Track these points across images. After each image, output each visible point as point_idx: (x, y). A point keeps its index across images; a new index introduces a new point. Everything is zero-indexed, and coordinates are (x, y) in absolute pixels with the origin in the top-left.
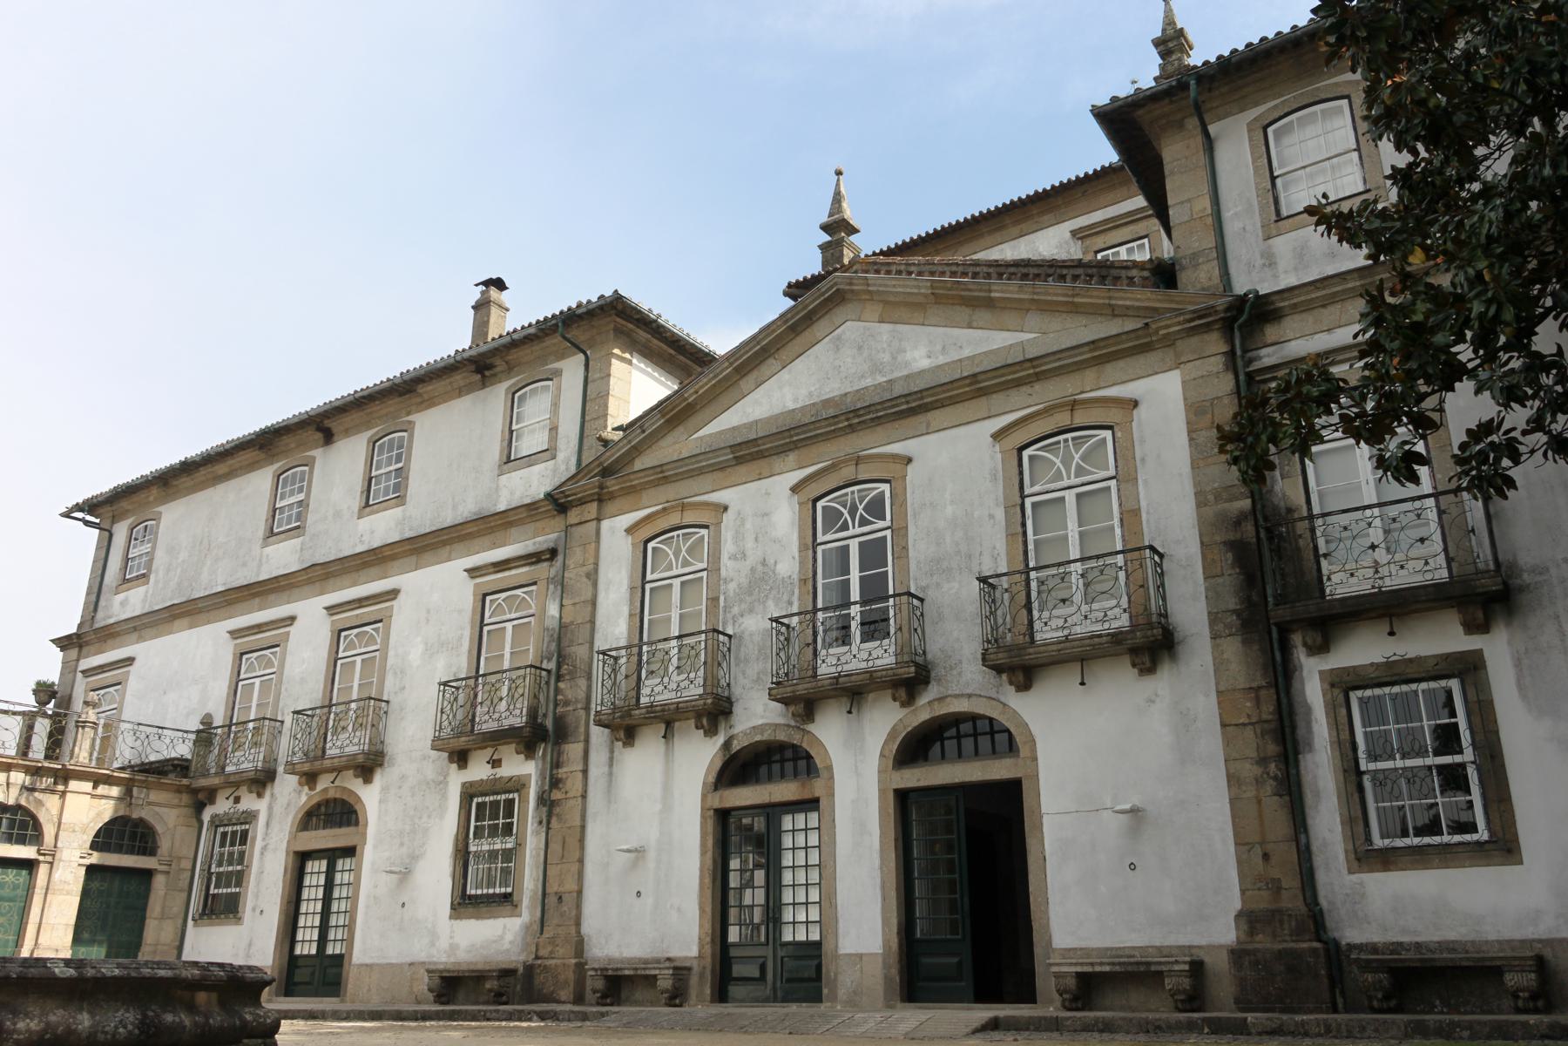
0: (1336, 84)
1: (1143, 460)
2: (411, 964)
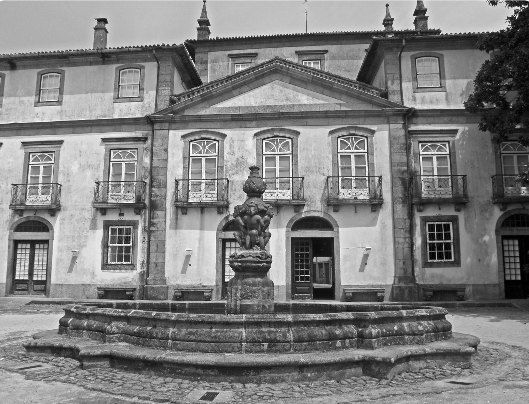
0: (435, 53)
1: (376, 149)
2: (82, 285)
